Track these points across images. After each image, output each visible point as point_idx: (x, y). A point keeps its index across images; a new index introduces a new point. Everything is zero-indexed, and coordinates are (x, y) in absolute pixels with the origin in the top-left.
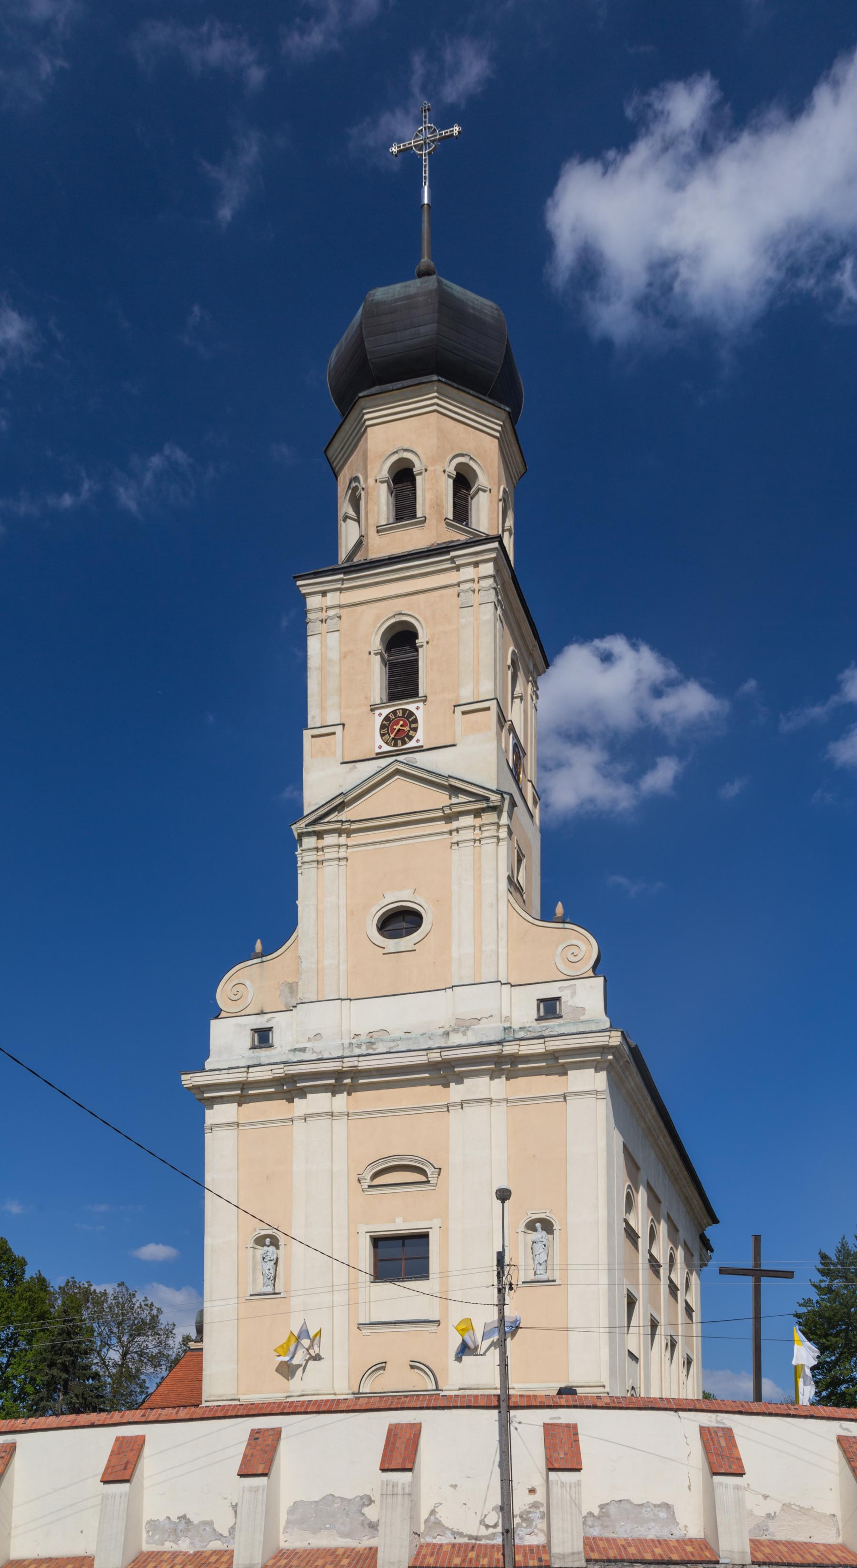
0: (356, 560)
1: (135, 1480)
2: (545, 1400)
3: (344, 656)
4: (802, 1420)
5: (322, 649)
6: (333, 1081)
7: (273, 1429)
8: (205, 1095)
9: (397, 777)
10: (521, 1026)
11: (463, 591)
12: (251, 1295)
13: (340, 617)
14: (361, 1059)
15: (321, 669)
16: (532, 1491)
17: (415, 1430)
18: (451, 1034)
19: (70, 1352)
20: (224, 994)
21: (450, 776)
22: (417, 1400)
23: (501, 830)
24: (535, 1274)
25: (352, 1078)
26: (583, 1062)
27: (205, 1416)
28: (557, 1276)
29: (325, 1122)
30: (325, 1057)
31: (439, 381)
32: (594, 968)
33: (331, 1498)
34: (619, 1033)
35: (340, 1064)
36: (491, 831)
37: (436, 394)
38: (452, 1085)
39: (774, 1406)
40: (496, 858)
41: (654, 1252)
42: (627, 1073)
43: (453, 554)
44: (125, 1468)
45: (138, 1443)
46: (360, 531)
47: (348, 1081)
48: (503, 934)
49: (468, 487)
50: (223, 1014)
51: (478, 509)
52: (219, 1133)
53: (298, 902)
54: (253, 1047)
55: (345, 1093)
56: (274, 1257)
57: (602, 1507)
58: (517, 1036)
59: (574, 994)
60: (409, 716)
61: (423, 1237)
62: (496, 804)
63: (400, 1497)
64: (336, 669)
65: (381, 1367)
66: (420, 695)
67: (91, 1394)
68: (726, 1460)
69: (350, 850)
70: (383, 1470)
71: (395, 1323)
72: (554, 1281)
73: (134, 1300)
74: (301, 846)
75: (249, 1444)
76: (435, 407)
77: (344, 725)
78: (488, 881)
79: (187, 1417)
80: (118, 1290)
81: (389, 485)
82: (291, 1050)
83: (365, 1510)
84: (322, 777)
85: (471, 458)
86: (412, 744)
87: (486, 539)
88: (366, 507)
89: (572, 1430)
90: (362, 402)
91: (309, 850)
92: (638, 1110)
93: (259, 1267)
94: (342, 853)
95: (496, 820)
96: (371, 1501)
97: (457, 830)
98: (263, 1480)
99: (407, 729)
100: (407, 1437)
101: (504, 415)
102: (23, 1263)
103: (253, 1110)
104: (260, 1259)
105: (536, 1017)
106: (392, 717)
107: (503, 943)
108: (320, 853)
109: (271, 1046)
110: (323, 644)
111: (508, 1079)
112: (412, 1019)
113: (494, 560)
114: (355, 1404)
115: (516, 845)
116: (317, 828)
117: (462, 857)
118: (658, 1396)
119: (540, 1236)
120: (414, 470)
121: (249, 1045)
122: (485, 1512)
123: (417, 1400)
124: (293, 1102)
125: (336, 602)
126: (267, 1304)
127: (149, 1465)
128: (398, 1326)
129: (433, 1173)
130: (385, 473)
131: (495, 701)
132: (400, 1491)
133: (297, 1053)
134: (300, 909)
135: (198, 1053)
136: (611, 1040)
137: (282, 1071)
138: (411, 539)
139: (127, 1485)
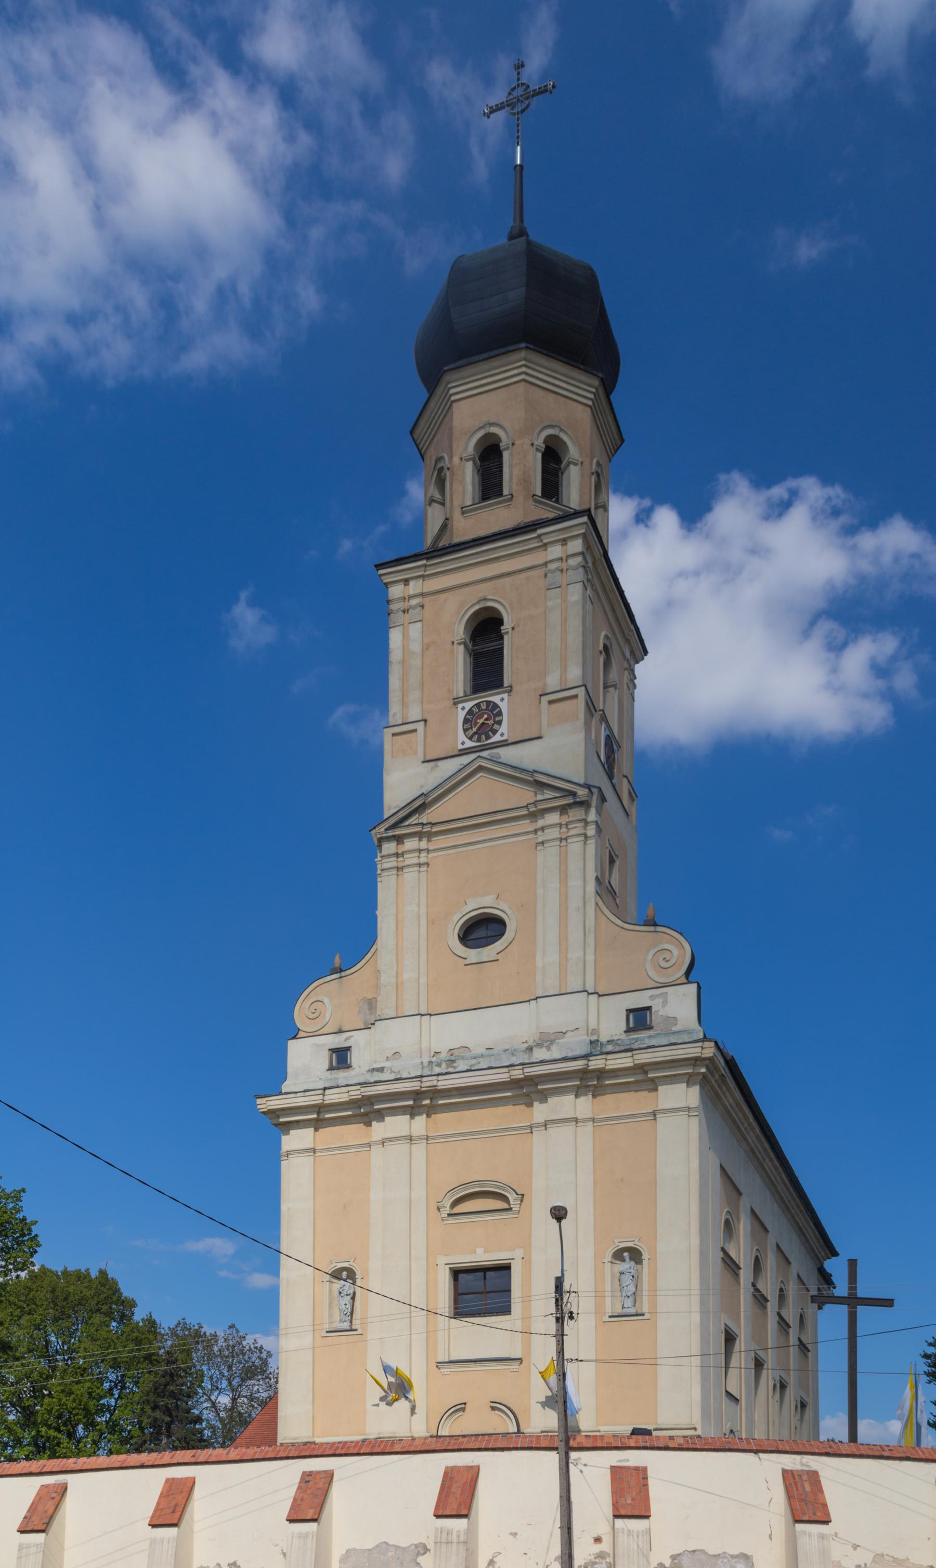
0: (440, 545)
1: (183, 1524)
2: (612, 1440)
3: (425, 648)
4: (897, 1462)
5: (404, 641)
6: (411, 1103)
7: (325, 1472)
8: (281, 1120)
9: (481, 774)
10: (609, 1039)
11: (550, 571)
13: (422, 606)
14: (441, 1078)
15: (403, 662)
16: (598, 1540)
17: (474, 1473)
18: (534, 1049)
19: (172, 1395)
20: (301, 1014)
21: (534, 771)
22: (475, 1441)
23: (588, 828)
24: (623, 1307)
25: (431, 1099)
26: (675, 1075)
27: (256, 1457)
28: (645, 1309)
29: (403, 1147)
30: (403, 1076)
31: (527, 348)
32: (688, 973)
33: (384, 1545)
34: (713, 1044)
35: (418, 1083)
36: (577, 829)
37: (523, 362)
38: (536, 1104)
39: (866, 1447)
40: (583, 858)
41: (760, 1286)
42: (724, 1088)
43: (540, 531)
44: (173, 1512)
45: (189, 1486)
46: (446, 514)
47: (427, 1102)
48: (591, 940)
49: (558, 460)
50: (301, 1034)
51: (569, 484)
52: (295, 1160)
53: (378, 913)
54: (331, 1068)
55: (425, 1116)
56: (351, 1291)
57: (674, 1557)
58: (604, 1050)
59: (665, 1003)
60: (493, 708)
61: (505, 1268)
62: (583, 799)
63: (454, 1546)
64: (418, 662)
65: (461, 1408)
66: (505, 685)
67: (194, 1437)
68: (811, 1507)
70: (438, 1516)
71: (475, 1361)
72: (643, 1315)
73: (244, 1343)
74: (381, 852)
75: (299, 1488)
76: (523, 377)
77: (425, 721)
78: (575, 883)
79: (238, 1458)
80: (228, 1332)
81: (474, 463)
82: (369, 1071)
83: (420, 1559)
85: (561, 430)
86: (496, 738)
87: (575, 514)
88: (451, 489)
89: (641, 1473)
90: (447, 377)
91: (389, 856)
92: (739, 1129)
93: (336, 1302)
94: (423, 858)
95: (584, 817)
96: (426, 1550)
97: (543, 829)
98: (314, 1525)
99: (490, 722)
100: (464, 1480)
101: (596, 382)
102: (132, 1304)
103: (331, 1135)
104: (336, 1293)
105: (625, 1029)
106: (476, 710)
107: (590, 950)
108: (401, 859)
109: (349, 1067)
110: (405, 635)
111: (594, 1096)
112: (493, 1032)
113: (584, 535)
114: (410, 1446)
115: (607, 845)
116: (398, 832)
117: (548, 857)
118: (763, 1437)
119: (628, 1266)
120: (501, 445)
121: (327, 1066)
122: (548, 1563)
123: (475, 1441)
124: (371, 1125)
125: (419, 591)
126: (344, 1338)
127: (200, 1507)
128: (478, 1364)
129: (515, 1200)
130: (471, 449)
131: (583, 688)
132: (455, 1539)
133: (375, 1073)
134: (379, 920)
135: (275, 1073)
136: (705, 1051)
137: (358, 1092)
138: (499, 517)
139: (175, 1530)
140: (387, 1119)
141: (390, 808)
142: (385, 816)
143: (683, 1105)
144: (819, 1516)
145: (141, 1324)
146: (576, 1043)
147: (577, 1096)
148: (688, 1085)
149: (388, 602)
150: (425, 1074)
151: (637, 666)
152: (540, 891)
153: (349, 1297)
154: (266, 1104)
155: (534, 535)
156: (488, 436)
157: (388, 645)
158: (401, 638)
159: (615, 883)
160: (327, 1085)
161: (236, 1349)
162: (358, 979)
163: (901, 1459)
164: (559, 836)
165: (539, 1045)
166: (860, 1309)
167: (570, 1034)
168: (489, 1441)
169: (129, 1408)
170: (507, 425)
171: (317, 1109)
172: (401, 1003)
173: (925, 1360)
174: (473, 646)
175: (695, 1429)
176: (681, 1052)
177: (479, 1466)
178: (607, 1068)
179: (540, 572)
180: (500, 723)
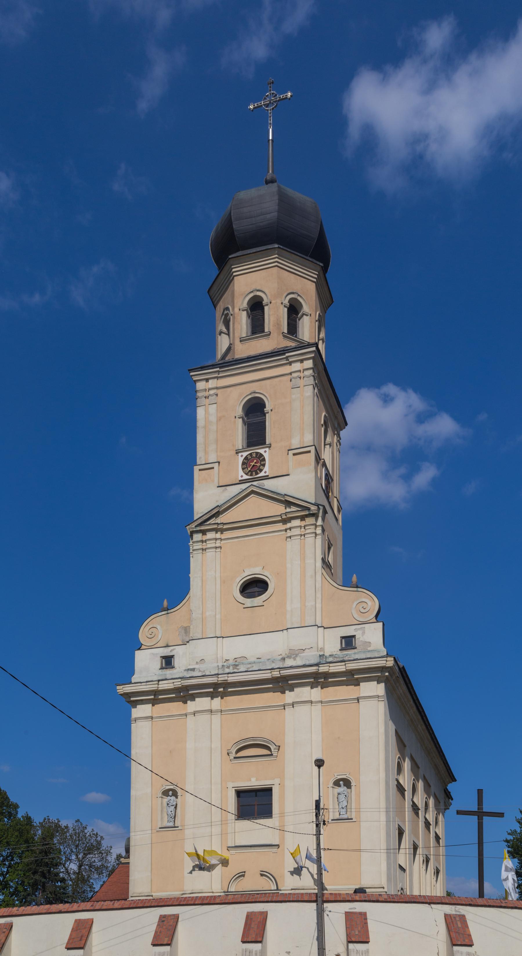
1: (87, 947)
2: (345, 896)
3: (219, 419)
7: (174, 915)
8: (132, 699)
10: (330, 654)
11: (294, 378)
13: (217, 395)
14: (230, 675)
15: (205, 427)
17: (264, 916)
18: (286, 659)
19: (47, 865)
21: (285, 495)
22: (264, 897)
23: (317, 529)
24: (340, 814)
25: (224, 688)
27: (131, 906)
28: (353, 816)
29: (207, 716)
30: (207, 674)
32: (377, 616)
34: (392, 659)
35: (216, 678)
36: (311, 529)
38: (287, 692)
39: (492, 901)
40: (314, 546)
42: (398, 685)
43: (287, 355)
44: (81, 940)
45: (90, 923)
46: (230, 341)
47: (221, 689)
48: (319, 595)
49: (297, 313)
50: (143, 647)
52: (140, 723)
53: (190, 575)
54: (162, 668)
55: (220, 698)
56: (175, 803)
59: (364, 633)
60: (260, 457)
62: (314, 512)
64: (214, 428)
65: (242, 875)
69: (223, 542)
70: (243, 942)
72: (352, 819)
73: (86, 831)
74: (192, 539)
75: (158, 925)
76: (276, 264)
77: (219, 463)
78: (309, 561)
79: (120, 907)
82: (185, 670)
84: (206, 496)
85: (299, 295)
86: (262, 474)
88: (233, 326)
89: (363, 916)
91: (197, 542)
95: (315, 522)
97: (290, 529)
99: (258, 465)
102: (16, 807)
104: (165, 804)
105: (340, 648)
106: (249, 457)
107: (319, 601)
108: (204, 544)
109: (173, 667)
110: (206, 411)
111: (322, 688)
112: (261, 649)
113: (313, 358)
115: (327, 538)
116: (203, 528)
117: (293, 546)
120: (263, 302)
123: (264, 897)
124: (186, 703)
125: (214, 386)
127: (96, 938)
129: (275, 749)
130: (245, 305)
131: (314, 447)
133: (189, 671)
134: (191, 579)
136: (388, 663)
137: (180, 683)
140: (197, 699)
141: (198, 513)
142: (195, 519)
143: (375, 694)
144: (467, 942)
145: (22, 819)
146: (311, 657)
147: (312, 688)
148: (378, 683)
149: (196, 391)
150: (219, 673)
151: (341, 432)
152: (289, 565)
153: (173, 807)
154: (122, 689)
156: (255, 297)
157: (196, 417)
158: (204, 412)
159: (331, 559)
160: (160, 678)
161: (80, 833)
162: (179, 614)
163: (512, 908)
164: (300, 533)
165: (289, 657)
166: (485, 819)
167: (307, 650)
168: (273, 896)
169: (16, 874)
170: (266, 291)
171: (154, 693)
172: (203, 630)
173: (506, 844)
174: (248, 419)
175: (383, 888)
177: (267, 912)
178: (330, 671)
180: (264, 465)
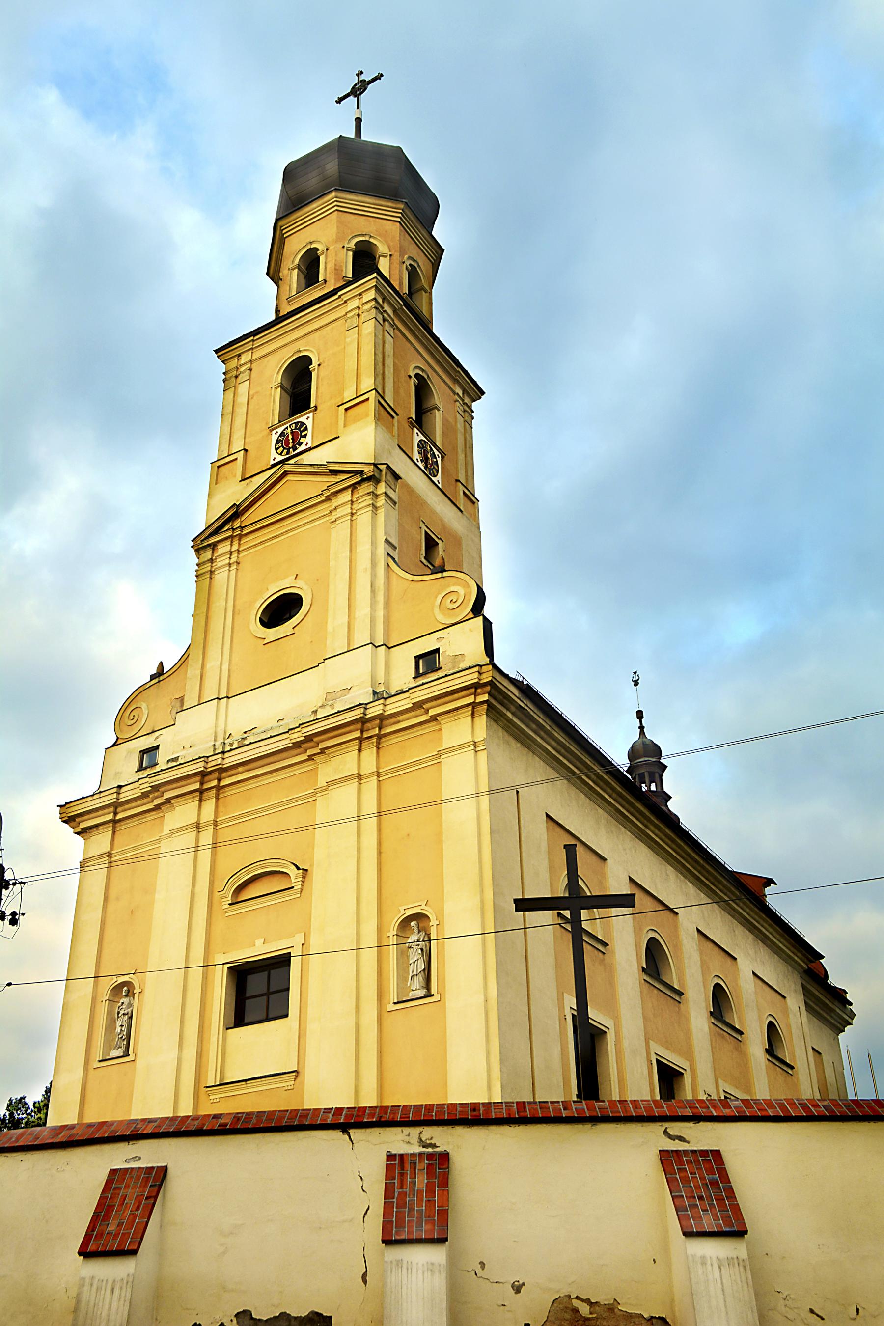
12: (100, 1061)
31: (336, 189)
43: (339, 293)
76: (336, 208)
116: (212, 540)
136: (484, 676)
152: (332, 563)
155: (336, 296)
171: (112, 809)
176: (457, 681)
179: (342, 321)
